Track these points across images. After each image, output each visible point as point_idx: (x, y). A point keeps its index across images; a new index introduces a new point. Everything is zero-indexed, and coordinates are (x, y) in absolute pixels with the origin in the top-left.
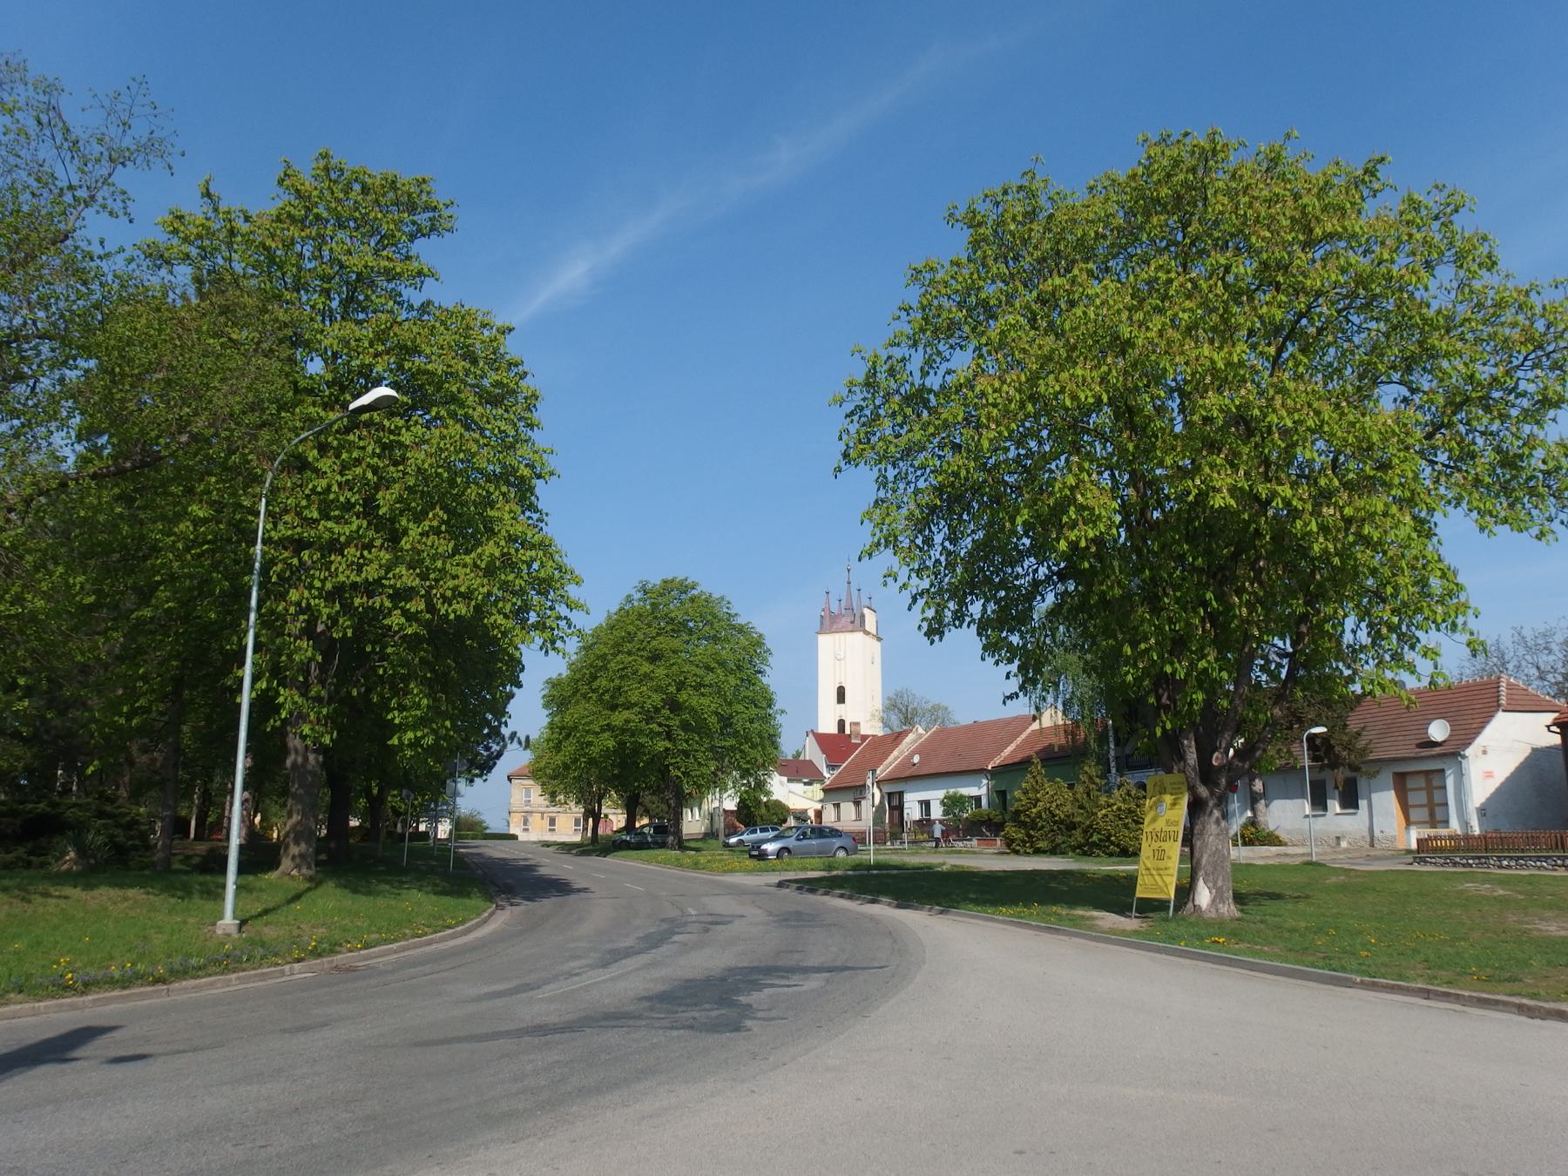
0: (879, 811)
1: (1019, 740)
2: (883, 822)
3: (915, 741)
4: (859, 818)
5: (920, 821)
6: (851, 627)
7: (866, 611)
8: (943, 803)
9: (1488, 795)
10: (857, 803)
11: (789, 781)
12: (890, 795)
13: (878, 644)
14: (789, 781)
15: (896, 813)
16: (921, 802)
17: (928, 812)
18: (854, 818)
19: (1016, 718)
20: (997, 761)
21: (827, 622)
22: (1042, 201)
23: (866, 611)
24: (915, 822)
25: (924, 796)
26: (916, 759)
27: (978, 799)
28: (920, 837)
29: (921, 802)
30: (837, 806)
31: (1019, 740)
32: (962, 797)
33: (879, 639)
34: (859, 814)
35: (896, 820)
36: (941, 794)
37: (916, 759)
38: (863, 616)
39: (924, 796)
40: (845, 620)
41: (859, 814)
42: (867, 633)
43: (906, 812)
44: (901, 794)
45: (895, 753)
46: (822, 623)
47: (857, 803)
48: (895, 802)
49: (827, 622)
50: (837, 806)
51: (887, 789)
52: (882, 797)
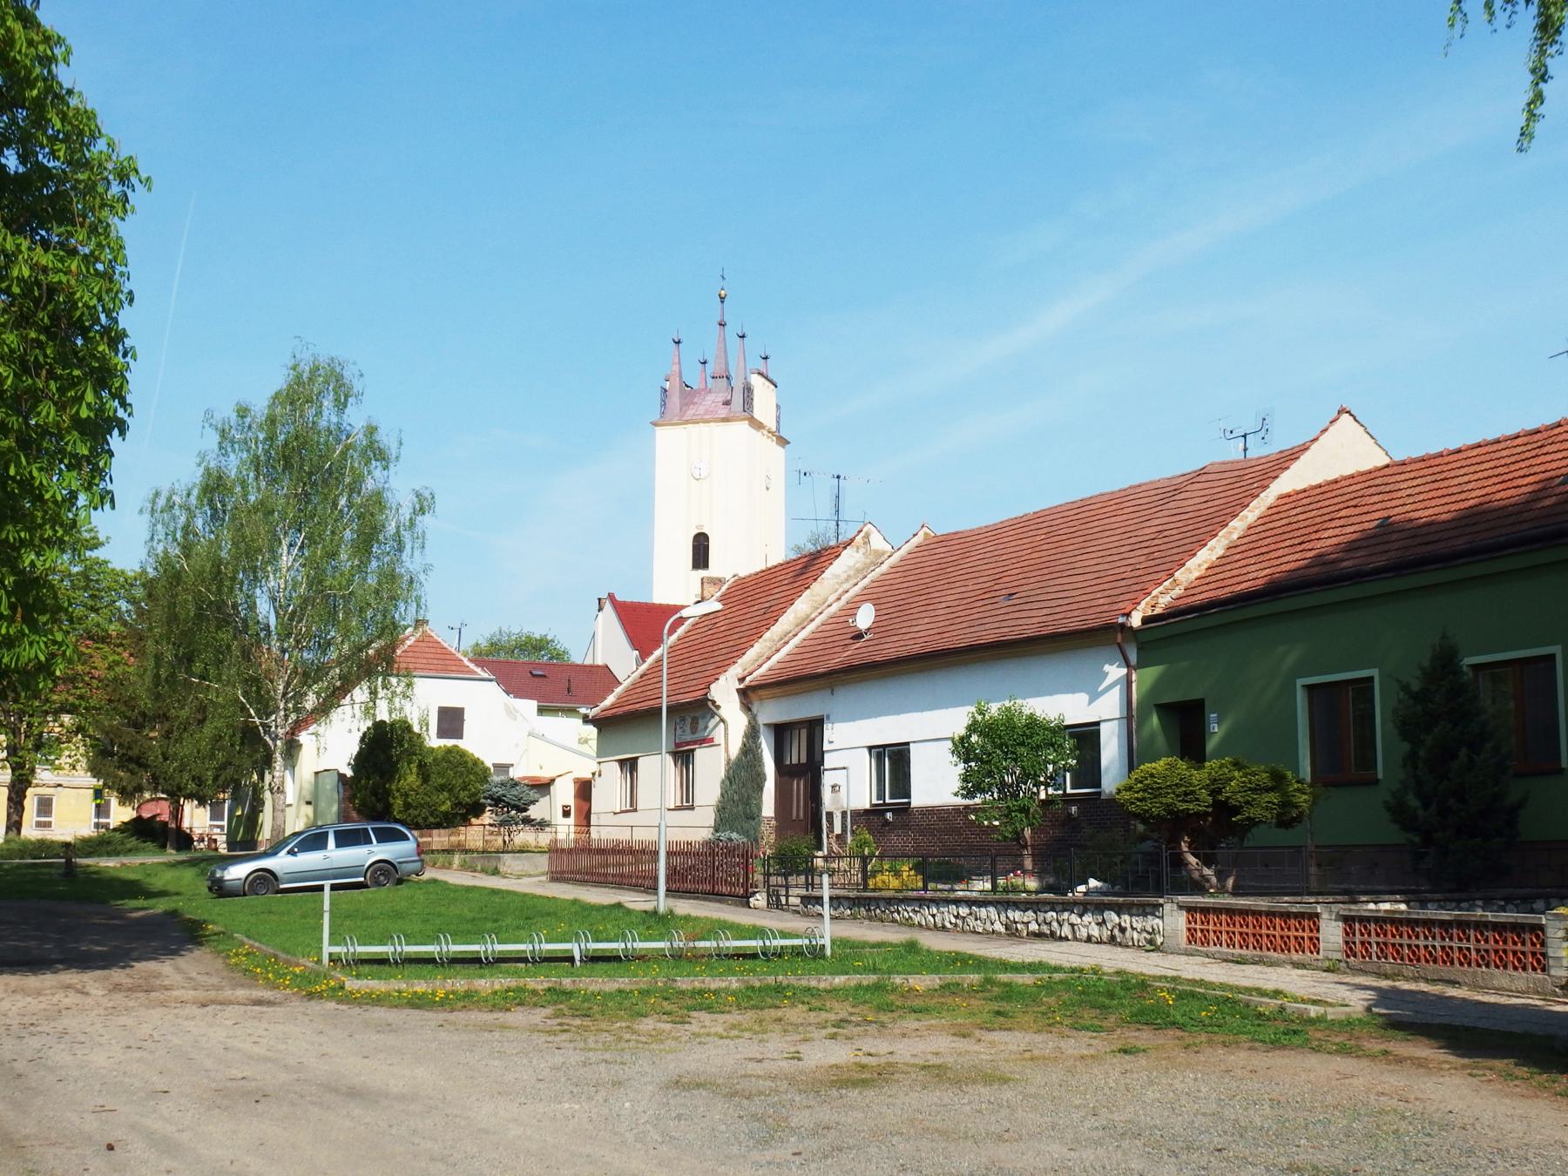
0: (743, 774)
1: (1237, 527)
2: (753, 815)
3: (862, 572)
4: (687, 804)
5: (875, 812)
6: (723, 412)
7: (757, 382)
8: (963, 748)
9: (944, 710)
10: (683, 757)
11: (542, 711)
12: (781, 732)
13: (780, 451)
14: (542, 711)
15: (799, 786)
16: (878, 752)
17: (902, 782)
18: (673, 799)
19: (1201, 472)
20: (1163, 598)
21: (675, 400)
22: (868, 561)
23: (757, 382)
24: (857, 814)
25: (888, 729)
26: (865, 618)
27: (1087, 736)
28: (887, 881)
29: (878, 752)
30: (630, 766)
31: (1237, 527)
32: (1033, 723)
33: (783, 442)
34: (687, 786)
35: (798, 810)
36: (955, 720)
37: (865, 618)
38: (748, 390)
39: (888, 729)
40: (713, 400)
41: (687, 786)
42: (757, 425)
43: (828, 779)
44: (814, 727)
45: (802, 606)
46: (664, 404)
47: (683, 757)
48: (797, 755)
49: (675, 400)
50: (630, 766)
51: (773, 712)
52: (752, 734)
